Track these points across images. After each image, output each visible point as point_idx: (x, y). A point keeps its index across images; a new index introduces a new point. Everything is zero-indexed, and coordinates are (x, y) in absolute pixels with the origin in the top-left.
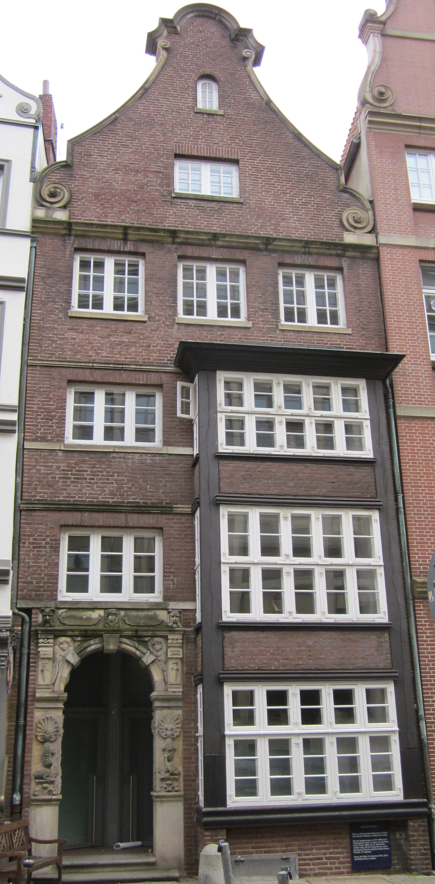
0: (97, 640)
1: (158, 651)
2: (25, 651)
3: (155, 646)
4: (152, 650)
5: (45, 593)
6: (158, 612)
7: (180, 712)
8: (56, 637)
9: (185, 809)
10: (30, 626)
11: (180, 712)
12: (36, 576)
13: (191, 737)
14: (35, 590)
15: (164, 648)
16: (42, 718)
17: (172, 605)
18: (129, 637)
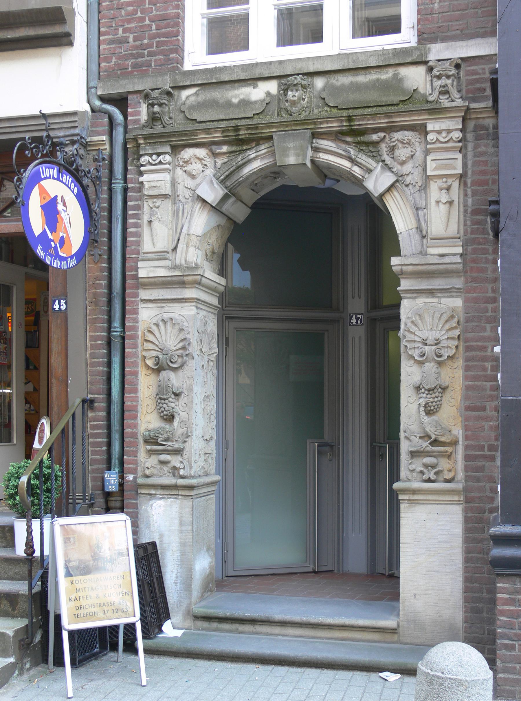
0: (263, 149)
1: (403, 163)
2: (118, 186)
3: (397, 152)
4: (388, 160)
5: (153, 58)
6: (404, 71)
7: (457, 303)
8: (176, 149)
9: (467, 520)
10: (126, 132)
11: (457, 303)
12: (132, 25)
13: (484, 359)
14: (132, 56)
15: (419, 155)
16: (154, 321)
17: (438, 51)
18: (337, 136)
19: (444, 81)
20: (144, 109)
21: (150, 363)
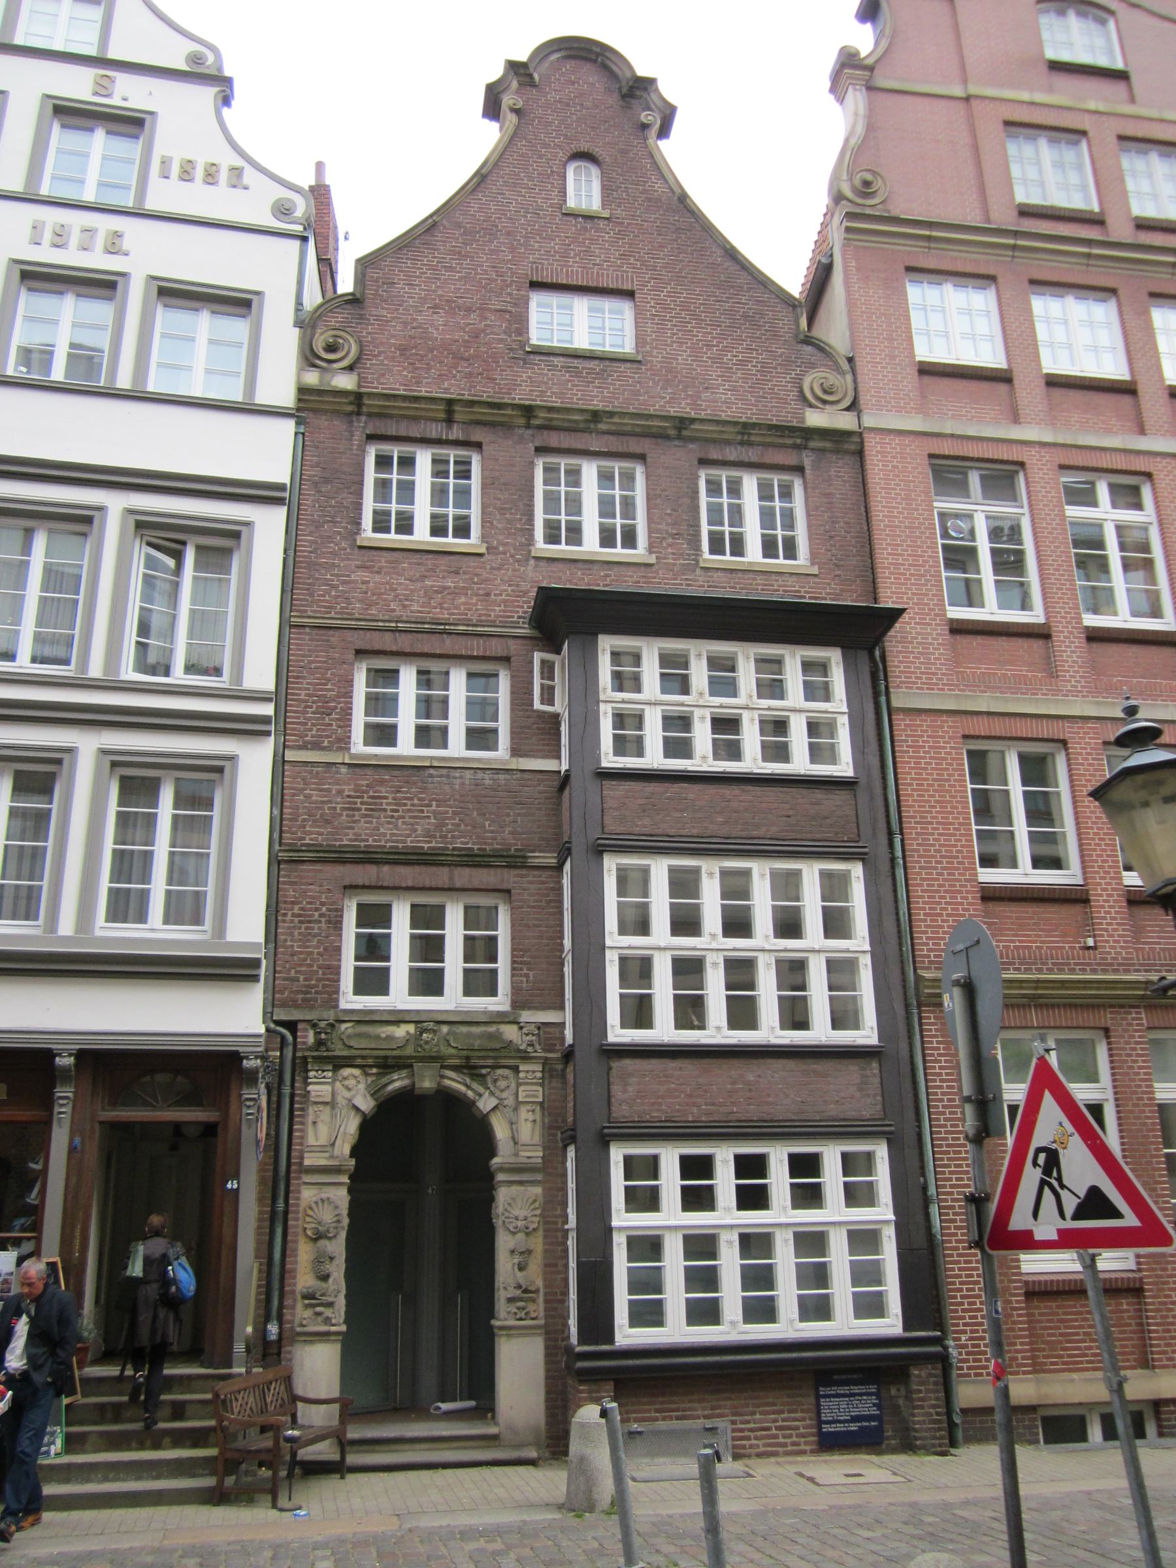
0: (404, 1073)
1: (502, 1091)
2: (287, 1090)
3: (499, 1083)
4: (492, 1088)
7: (538, 1190)
8: (337, 1068)
9: (547, 1347)
10: (295, 1050)
13: (557, 1230)
15: (513, 1085)
16: (314, 1199)
17: (526, 1016)
18: (455, 1068)
19: (530, 1038)
20: (311, 1034)
21: (309, 1233)
